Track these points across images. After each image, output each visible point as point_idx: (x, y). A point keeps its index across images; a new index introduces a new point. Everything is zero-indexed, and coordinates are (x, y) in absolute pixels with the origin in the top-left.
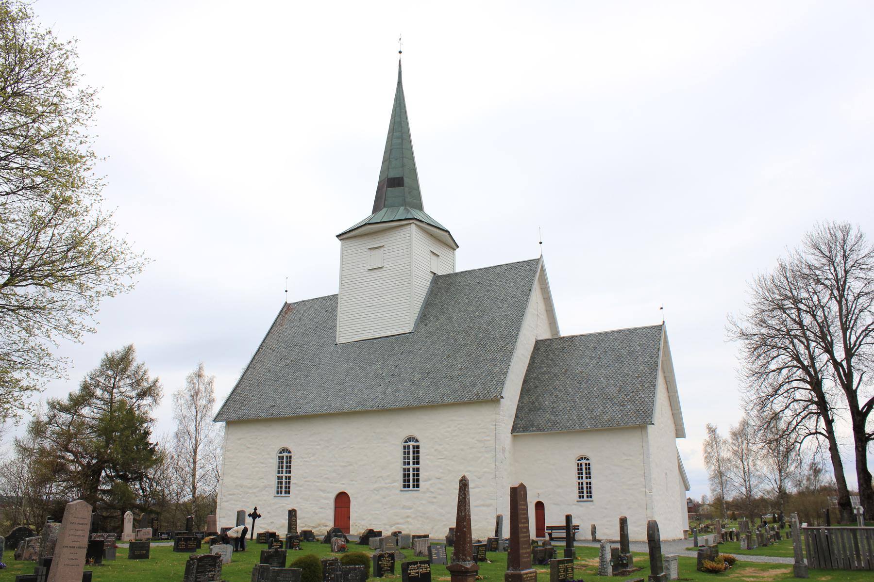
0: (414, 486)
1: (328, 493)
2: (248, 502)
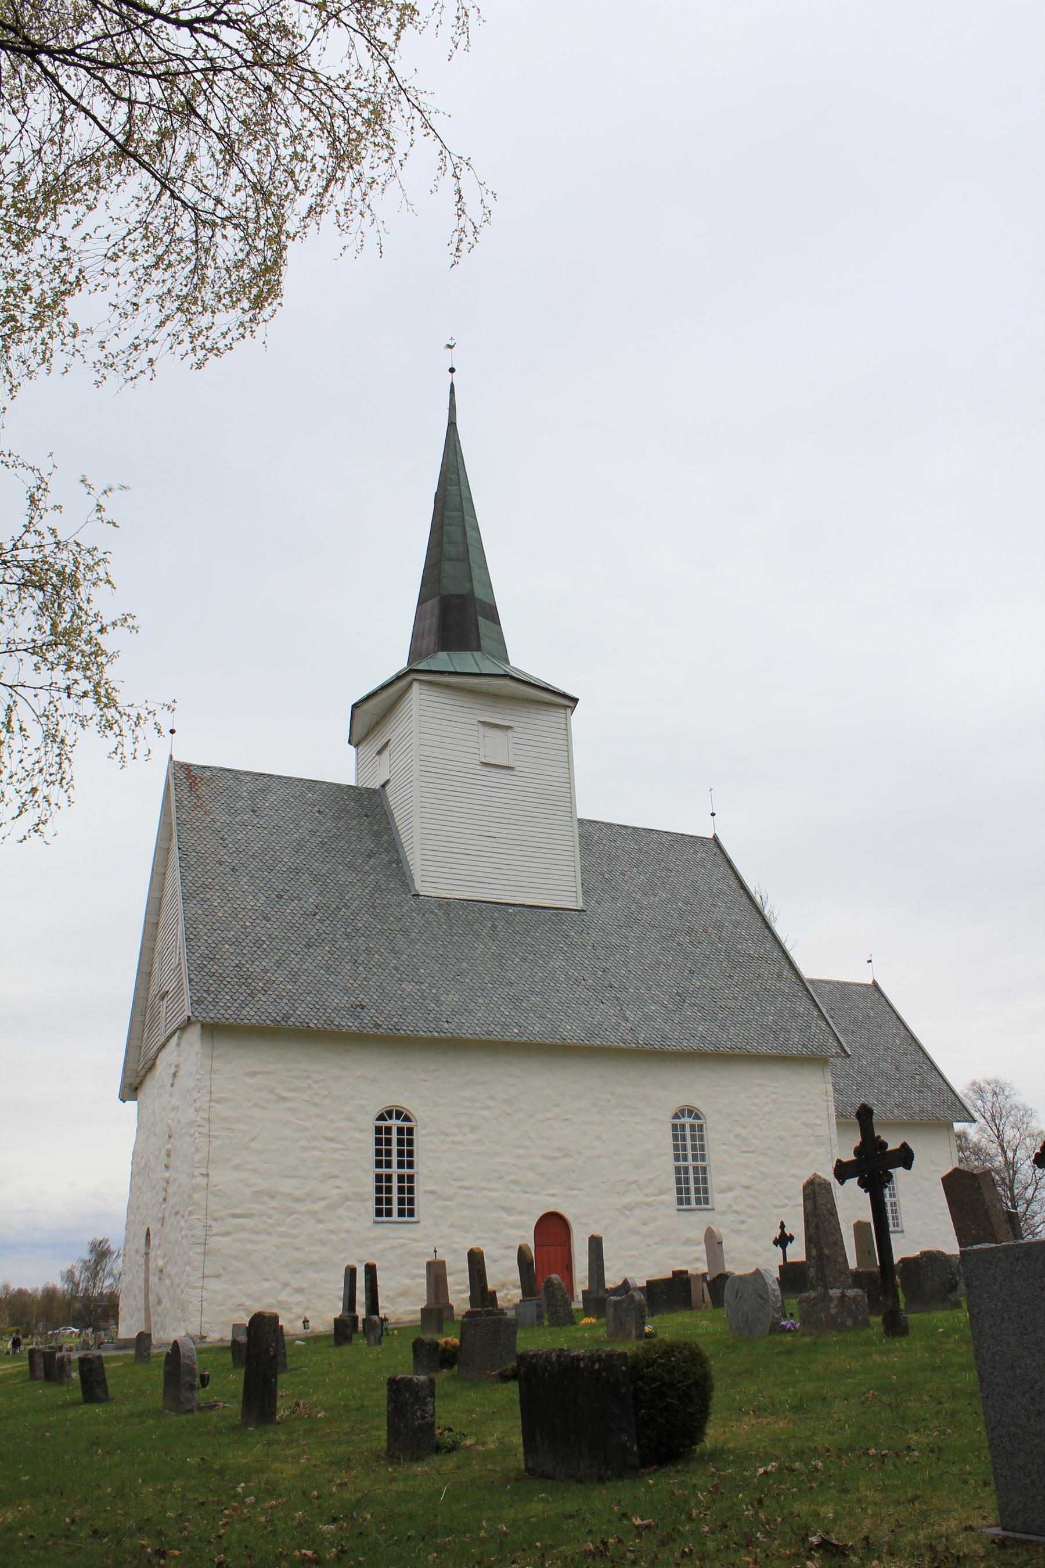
0: (401, 1213)
1: (521, 1213)
2: (295, 1237)
